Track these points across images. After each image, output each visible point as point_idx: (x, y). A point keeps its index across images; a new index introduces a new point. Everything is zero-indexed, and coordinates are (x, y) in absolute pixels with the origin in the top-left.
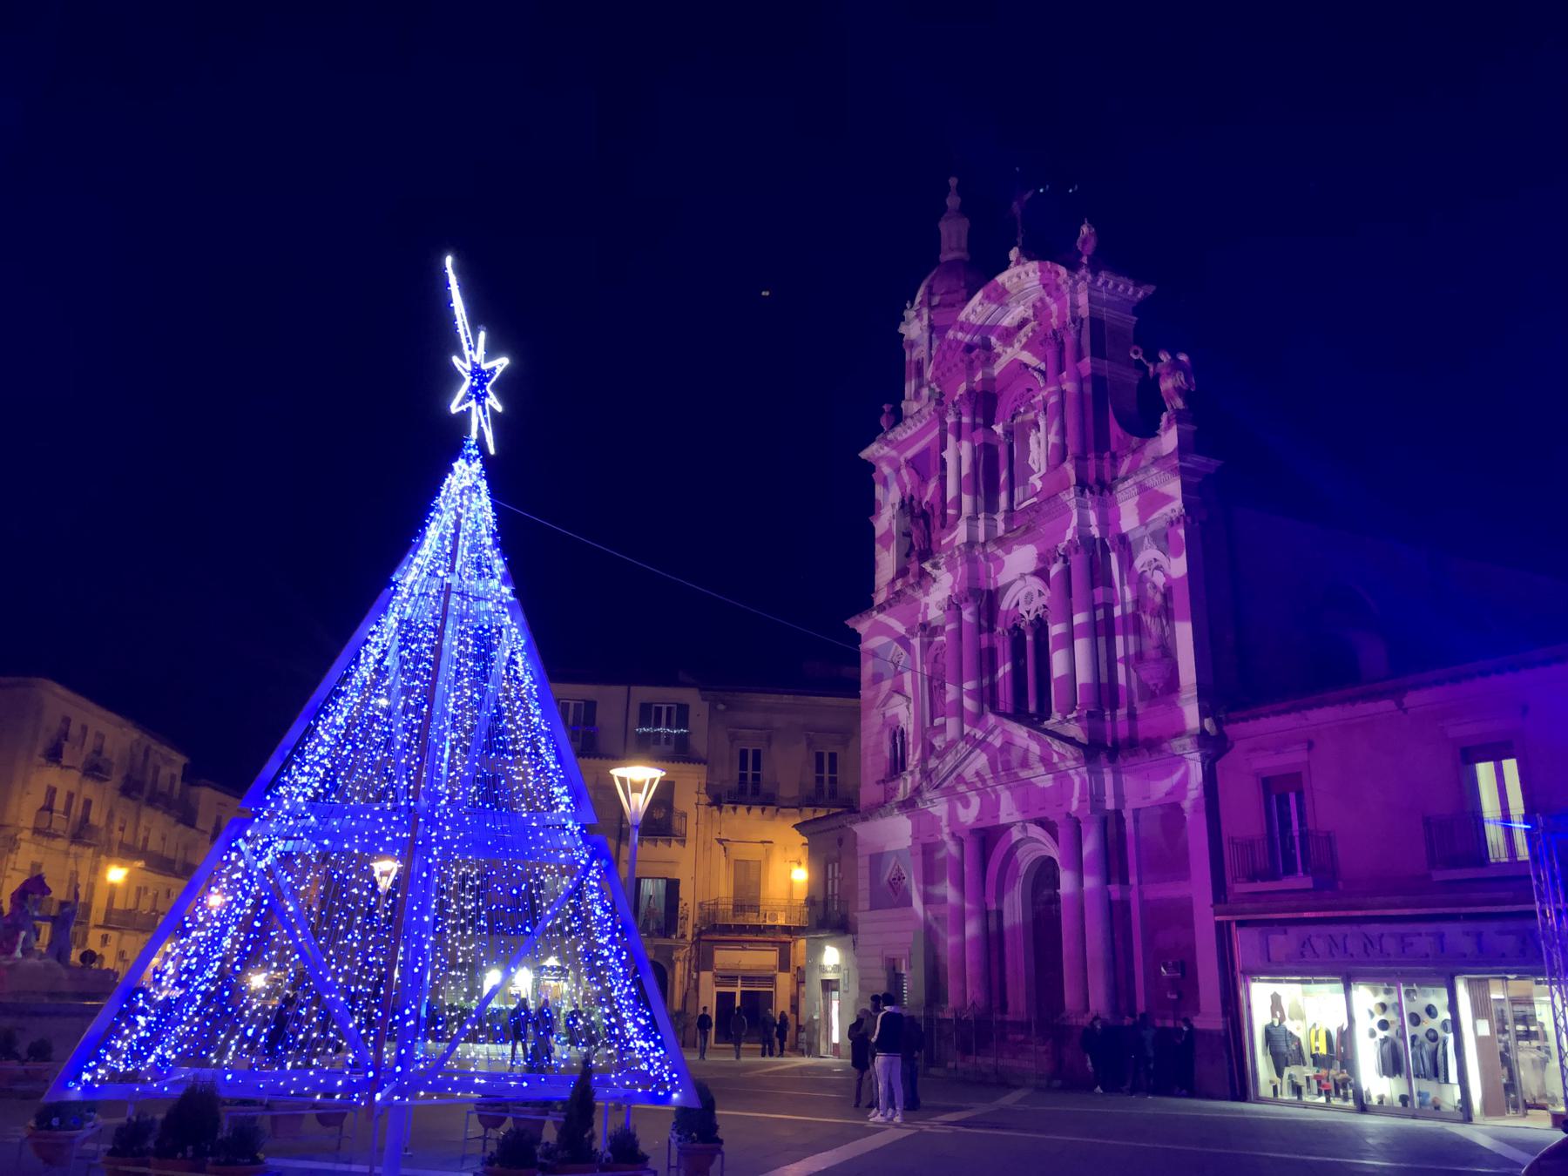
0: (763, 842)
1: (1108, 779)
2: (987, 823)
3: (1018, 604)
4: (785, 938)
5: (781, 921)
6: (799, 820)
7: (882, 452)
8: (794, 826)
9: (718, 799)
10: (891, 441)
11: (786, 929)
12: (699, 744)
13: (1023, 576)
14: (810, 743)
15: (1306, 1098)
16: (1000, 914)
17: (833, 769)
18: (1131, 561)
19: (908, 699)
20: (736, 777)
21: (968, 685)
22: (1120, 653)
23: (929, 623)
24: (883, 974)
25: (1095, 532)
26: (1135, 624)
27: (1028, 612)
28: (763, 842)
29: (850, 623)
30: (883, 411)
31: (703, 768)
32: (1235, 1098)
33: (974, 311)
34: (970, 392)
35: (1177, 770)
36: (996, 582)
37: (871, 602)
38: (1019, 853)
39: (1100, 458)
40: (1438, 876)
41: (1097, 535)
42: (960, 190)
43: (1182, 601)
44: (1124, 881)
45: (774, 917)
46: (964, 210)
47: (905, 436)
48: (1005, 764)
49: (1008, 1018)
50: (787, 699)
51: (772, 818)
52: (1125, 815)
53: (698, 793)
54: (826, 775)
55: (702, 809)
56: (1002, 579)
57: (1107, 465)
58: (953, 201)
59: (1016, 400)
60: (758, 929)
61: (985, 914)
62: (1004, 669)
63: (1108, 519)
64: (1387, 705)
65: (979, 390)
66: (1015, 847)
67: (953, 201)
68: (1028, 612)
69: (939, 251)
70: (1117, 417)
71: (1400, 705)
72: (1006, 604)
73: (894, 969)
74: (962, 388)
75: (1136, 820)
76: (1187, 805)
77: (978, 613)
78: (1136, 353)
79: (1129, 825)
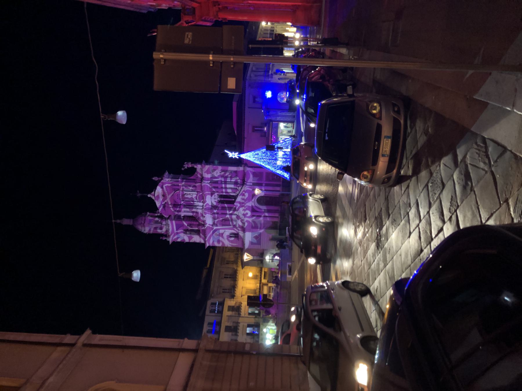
0: (242, 288)
1: (248, 184)
2: (251, 209)
3: (215, 201)
4: (262, 284)
5: (258, 285)
6: (241, 267)
8: (242, 269)
9: (233, 296)
10: (171, 235)
11: (260, 283)
12: (221, 300)
13: (211, 199)
16: (264, 210)
17: (228, 275)
18: (216, 177)
19: (225, 231)
20: (228, 293)
21: (228, 212)
22: (230, 180)
23: (212, 225)
24: (273, 242)
25: (209, 182)
26: (226, 177)
28: (242, 288)
29: (206, 247)
30: (162, 239)
31: (226, 299)
34: (172, 207)
35: (249, 173)
36: (210, 206)
37: (202, 244)
38: (256, 205)
39: (197, 180)
40: (267, 136)
41: (210, 181)
43: (225, 168)
44: (262, 183)
45: (257, 286)
47: (171, 231)
48: (242, 204)
49: (280, 209)
50: (212, 282)
51: (238, 287)
52: (253, 182)
53: (231, 301)
54: (229, 276)
55: (234, 300)
56: (210, 204)
57: (198, 179)
59: (178, 198)
60: (260, 289)
62: (226, 205)
63: (208, 179)
64: (245, 139)
65: (173, 206)
69: (129, 225)
70: (189, 177)
71: (246, 138)
72: (215, 204)
74: (172, 209)
75: (254, 181)
76: (253, 171)
77: (215, 209)
79: (255, 182)
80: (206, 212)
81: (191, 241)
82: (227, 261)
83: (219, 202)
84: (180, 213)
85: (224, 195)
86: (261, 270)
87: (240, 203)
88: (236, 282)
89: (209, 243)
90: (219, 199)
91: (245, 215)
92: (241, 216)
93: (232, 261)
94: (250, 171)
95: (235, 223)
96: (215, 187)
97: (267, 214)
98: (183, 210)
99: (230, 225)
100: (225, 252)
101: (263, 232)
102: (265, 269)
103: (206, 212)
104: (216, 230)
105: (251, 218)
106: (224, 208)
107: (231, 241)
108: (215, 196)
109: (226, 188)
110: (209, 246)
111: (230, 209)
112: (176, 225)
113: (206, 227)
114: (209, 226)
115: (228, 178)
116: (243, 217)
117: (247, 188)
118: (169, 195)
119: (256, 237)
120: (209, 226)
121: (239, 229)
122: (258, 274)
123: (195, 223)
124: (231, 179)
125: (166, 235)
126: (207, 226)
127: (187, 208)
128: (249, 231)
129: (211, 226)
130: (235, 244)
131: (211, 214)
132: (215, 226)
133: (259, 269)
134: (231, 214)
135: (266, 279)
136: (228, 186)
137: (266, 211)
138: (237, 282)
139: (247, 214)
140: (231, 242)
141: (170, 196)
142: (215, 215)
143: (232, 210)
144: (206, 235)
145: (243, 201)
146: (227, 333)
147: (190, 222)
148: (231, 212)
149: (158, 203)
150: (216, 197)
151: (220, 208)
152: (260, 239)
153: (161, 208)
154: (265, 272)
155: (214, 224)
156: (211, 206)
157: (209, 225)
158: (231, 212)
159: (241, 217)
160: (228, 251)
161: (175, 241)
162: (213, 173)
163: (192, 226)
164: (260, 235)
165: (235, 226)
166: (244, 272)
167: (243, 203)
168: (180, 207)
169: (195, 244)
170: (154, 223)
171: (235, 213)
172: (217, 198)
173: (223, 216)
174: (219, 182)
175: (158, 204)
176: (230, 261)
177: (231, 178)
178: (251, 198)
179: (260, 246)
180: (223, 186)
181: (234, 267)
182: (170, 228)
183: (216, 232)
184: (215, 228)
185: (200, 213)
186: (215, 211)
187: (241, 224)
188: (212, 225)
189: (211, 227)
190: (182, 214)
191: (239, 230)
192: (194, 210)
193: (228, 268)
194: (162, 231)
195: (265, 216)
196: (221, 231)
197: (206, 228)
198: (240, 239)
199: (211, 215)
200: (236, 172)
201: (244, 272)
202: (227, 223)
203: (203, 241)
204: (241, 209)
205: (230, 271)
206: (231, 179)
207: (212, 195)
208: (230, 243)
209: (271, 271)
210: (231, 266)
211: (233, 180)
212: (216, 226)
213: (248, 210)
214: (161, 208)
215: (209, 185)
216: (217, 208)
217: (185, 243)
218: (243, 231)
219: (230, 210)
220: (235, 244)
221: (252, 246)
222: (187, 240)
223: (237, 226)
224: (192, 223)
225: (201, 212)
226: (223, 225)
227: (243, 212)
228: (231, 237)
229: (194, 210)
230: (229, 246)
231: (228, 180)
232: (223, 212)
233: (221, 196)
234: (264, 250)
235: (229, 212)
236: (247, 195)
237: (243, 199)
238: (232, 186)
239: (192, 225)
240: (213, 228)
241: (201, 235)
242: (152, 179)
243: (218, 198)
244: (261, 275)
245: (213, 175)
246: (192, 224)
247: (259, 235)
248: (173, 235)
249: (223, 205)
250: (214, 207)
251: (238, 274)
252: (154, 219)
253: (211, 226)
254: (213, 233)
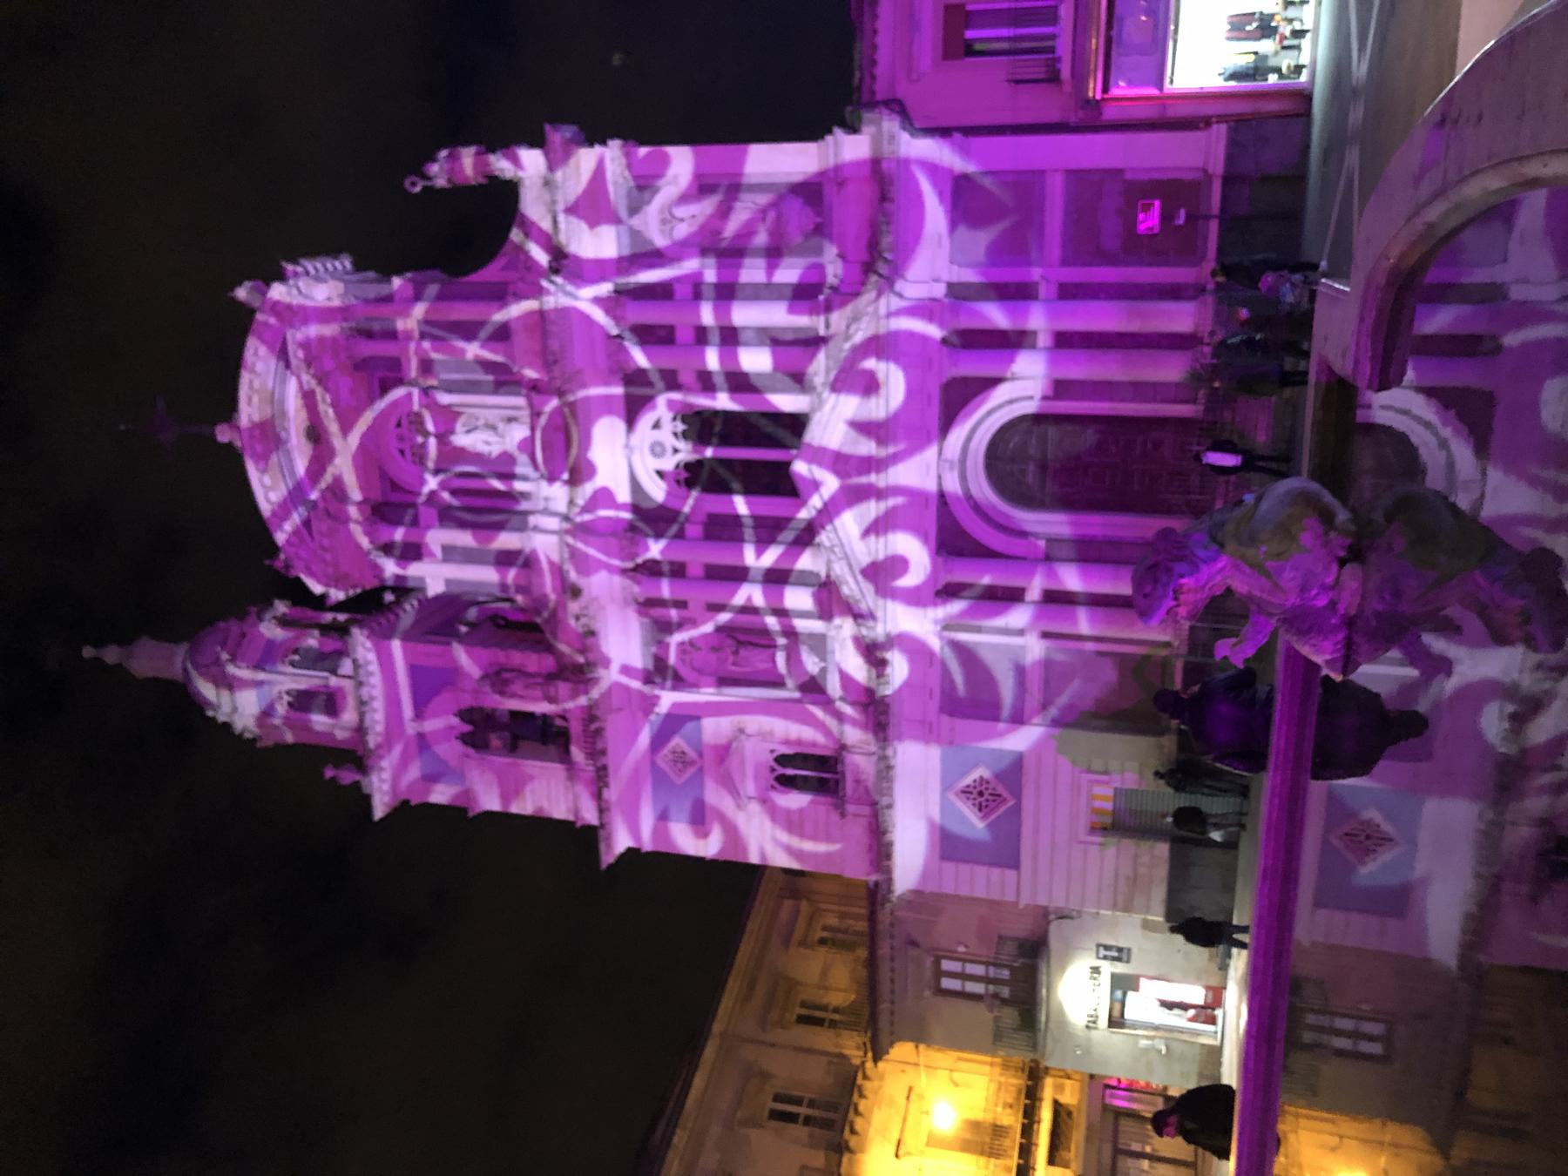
7: (386, 775)
13: (627, 446)
14: (752, 1122)
15: (1308, 25)
16: (1051, 541)
17: (798, 1102)
27: (676, 451)
30: (333, 779)
32: (1307, 113)
33: (267, 489)
38: (975, 492)
42: (99, 644)
46: (126, 640)
47: (380, 728)
50: (680, 1138)
54: (803, 1111)
56: (624, 495)
58: (111, 655)
59: (402, 452)
61: (1048, 558)
66: (969, 497)
67: (111, 655)
68: (676, 451)
72: (657, 492)
73: (1105, 829)
78: (414, 184)
80: (586, 555)
81: (515, 809)
82: (803, 1005)
83: (691, 476)
84: (414, 570)
85: (728, 415)
86: (1032, 1096)
87: (839, 462)
88: (845, 1159)
89: (635, 830)
90: (686, 452)
91: (882, 573)
92: (853, 587)
93: (836, 1010)
94: (933, 170)
95: (812, 664)
96: (649, 336)
97: (1072, 579)
98: (437, 538)
99: (778, 683)
100: (803, 943)
101: (1040, 745)
102: (1059, 1088)
103: (592, 552)
104: (676, 721)
105: (935, 604)
106: (724, 529)
107: (788, 812)
108: (657, 426)
109: (730, 337)
110: (629, 850)
111: (767, 531)
112: (414, 671)
113: (603, 685)
114: (624, 680)
115: (747, 261)
116: (868, 588)
117: (889, 315)
118: (346, 429)
119: (983, 797)
120: (624, 680)
121: (848, 710)
122: (1012, 1120)
123: (534, 662)
124: (771, 268)
125: (355, 756)
126: (610, 676)
127: (462, 525)
128: (928, 734)
129: (636, 684)
130: (821, 848)
131: (624, 572)
132: (669, 683)
133: (1017, 1082)
134: (777, 578)
135: (1066, 1165)
136: (744, 315)
137: (1068, 551)
138: (851, 1162)
139: (898, 564)
140: (791, 822)
141: (354, 439)
142: (659, 589)
143: (781, 543)
144: (603, 752)
145: (867, 447)
146: (1322, 914)
147: (500, 656)
148: (770, 557)
149: (267, 480)
150: (666, 436)
151: (694, 530)
152: (1017, 810)
153: (288, 527)
154: (1058, 1107)
155: (659, 672)
156: (635, 508)
157: (626, 670)
158: (770, 557)
159: (845, 590)
160: (823, 942)
161: (413, 803)
162: (636, 222)
163: (506, 682)
164: (1014, 772)
165: (813, 688)
166: (910, 1089)
167: (870, 464)
168: (415, 522)
169: (539, 823)
170: (293, 664)
171: (806, 561)
172: (670, 441)
173: (714, 593)
174: (682, 291)
175: (267, 490)
176: (824, 1008)
177: (774, 254)
178: (934, 412)
179: (1011, 874)
180: (707, 315)
181: (847, 1052)
182: (372, 698)
183: (677, 742)
184: (668, 699)
185: (545, 566)
186: (655, 549)
187: (857, 668)
188: (648, 679)
189: (640, 692)
190: (434, 577)
191: (840, 717)
192: (506, 540)
193: (810, 1051)
194: (333, 726)
195: (1056, 599)
196: (714, 729)
197: (595, 693)
198: (850, 808)
199: (628, 582)
200: (809, 192)
201: (910, 1089)
202: (754, 660)
203: (590, 816)
204: (850, 523)
205: (814, 1077)
206: (771, 268)
207: (632, 411)
208: (784, 837)
209: (1106, 1108)
210: (823, 1039)
211: (788, 274)
212: (674, 688)
213: (918, 530)
214: (288, 527)
215: (599, 315)
216: (674, 529)
217: (471, 814)
218: (876, 733)
219: (762, 544)
220: (821, 848)
221: (949, 867)
222: (490, 801)
223: (834, 687)
224: (517, 658)
225: (555, 558)
226: (724, 681)
227: (866, 551)
228: (787, 783)
229: (506, 540)
230: (781, 860)
231: (752, 272)
232: (719, 556)
233: (700, 426)
234: (1044, 917)
235: (759, 553)
236: (895, 383)
237: (864, 428)
238: (777, 315)
239: (507, 675)
240: (653, 701)
241: (577, 754)
242: (234, 300)
243: (682, 445)
244: (1028, 1130)
245: (635, 235)
246: (512, 670)
247: (999, 776)
248: (397, 750)
249: (715, 504)
250: (651, 518)
251: (863, 1105)
252: (297, 638)
253: (636, 684)
254: (658, 741)
